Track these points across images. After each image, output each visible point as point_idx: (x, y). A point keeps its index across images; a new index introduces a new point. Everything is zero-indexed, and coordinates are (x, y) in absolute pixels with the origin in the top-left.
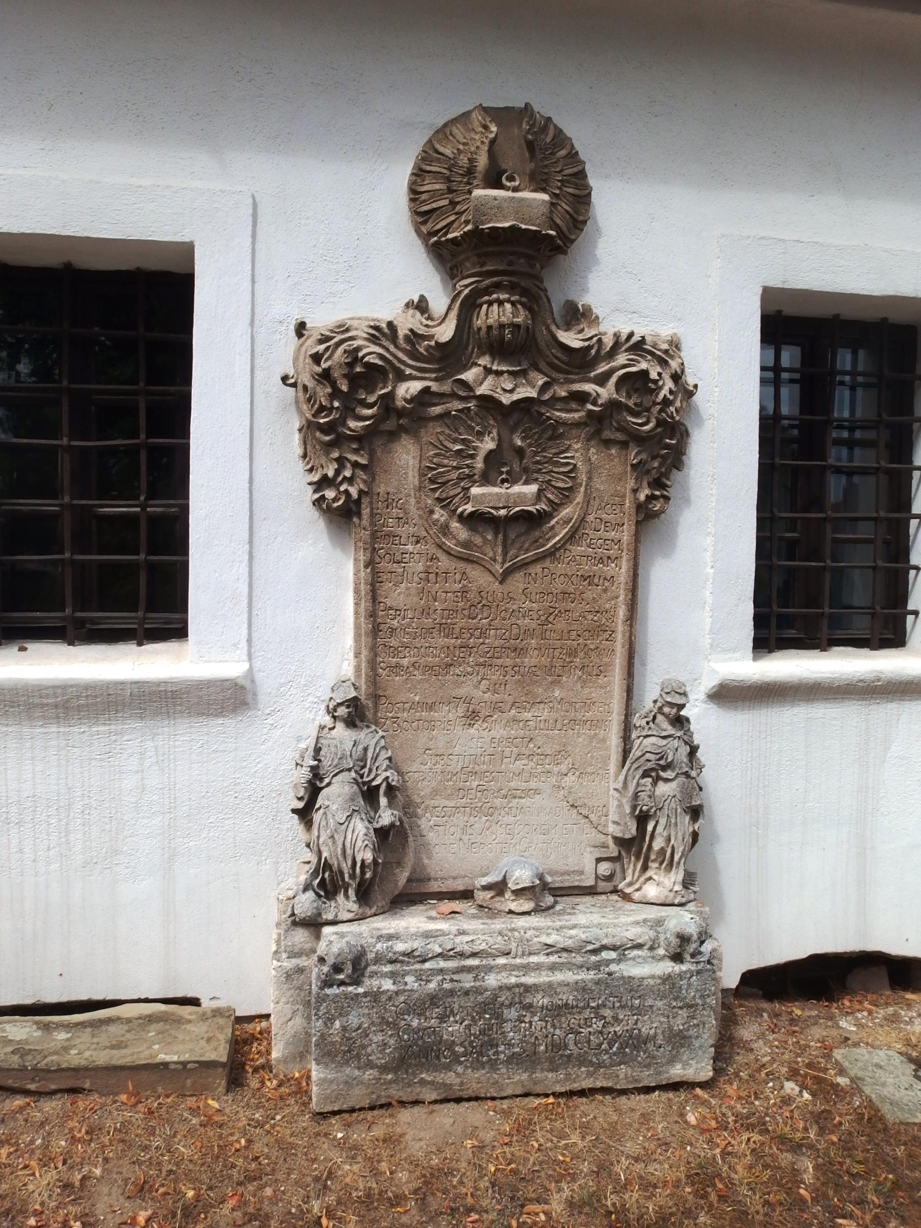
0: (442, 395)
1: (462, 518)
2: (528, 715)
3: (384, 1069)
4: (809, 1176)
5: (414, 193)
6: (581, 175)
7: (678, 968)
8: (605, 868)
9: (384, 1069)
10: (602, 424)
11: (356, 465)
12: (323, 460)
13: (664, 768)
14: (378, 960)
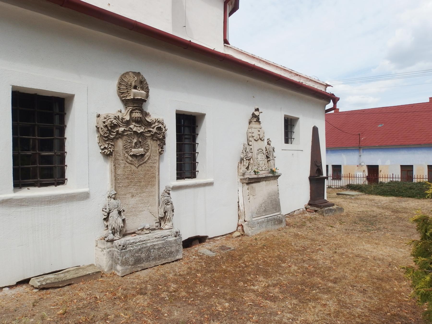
0: (127, 130)
1: (130, 156)
2: (142, 195)
3: (132, 265)
4: (204, 264)
5: (119, 88)
6: (148, 87)
7: (176, 238)
8: (157, 224)
9: (132, 265)
10: (154, 137)
11: (112, 145)
12: (104, 144)
13: (168, 202)
14: (128, 245)
